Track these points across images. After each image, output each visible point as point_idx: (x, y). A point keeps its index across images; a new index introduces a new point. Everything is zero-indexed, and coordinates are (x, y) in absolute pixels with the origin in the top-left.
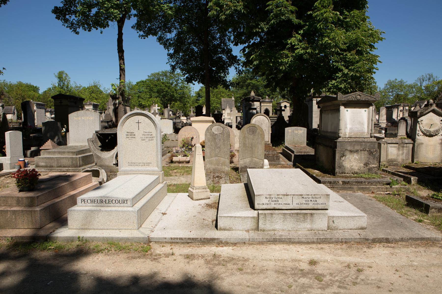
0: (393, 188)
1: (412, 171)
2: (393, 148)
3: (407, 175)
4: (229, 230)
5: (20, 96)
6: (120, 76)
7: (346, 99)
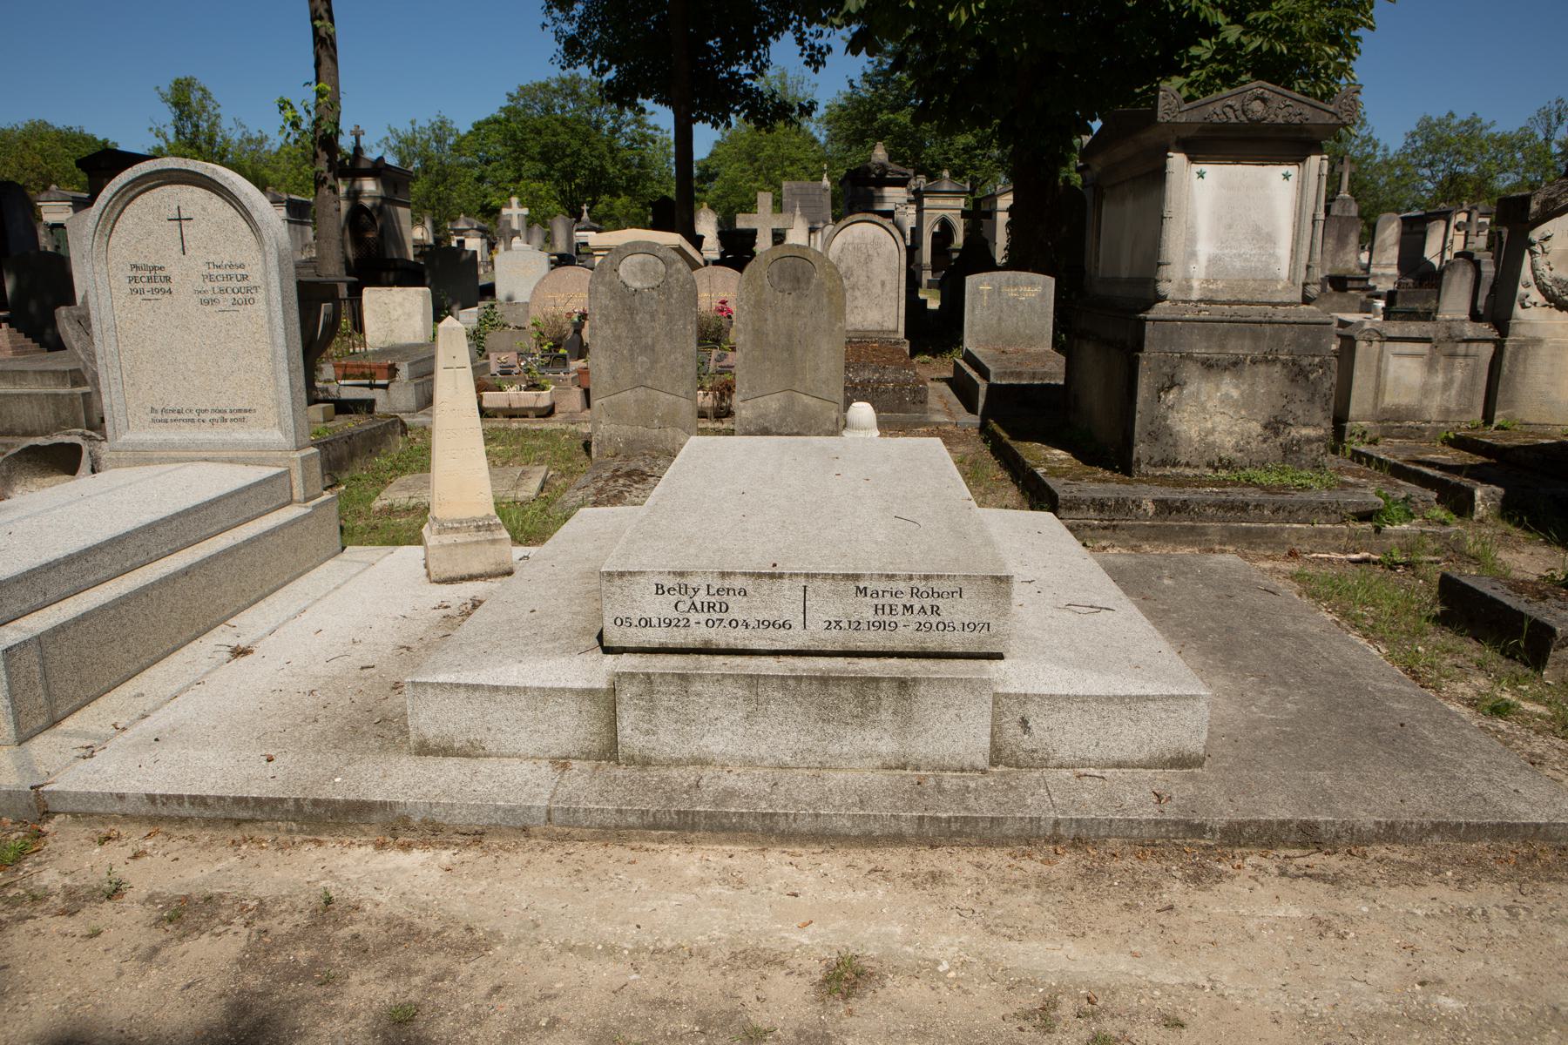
0: (1388, 536)
1: (1479, 459)
2: (1407, 361)
3: (1455, 479)
4: (470, 752)
5: (33, 176)
6: (318, 65)
7: (1196, 117)
